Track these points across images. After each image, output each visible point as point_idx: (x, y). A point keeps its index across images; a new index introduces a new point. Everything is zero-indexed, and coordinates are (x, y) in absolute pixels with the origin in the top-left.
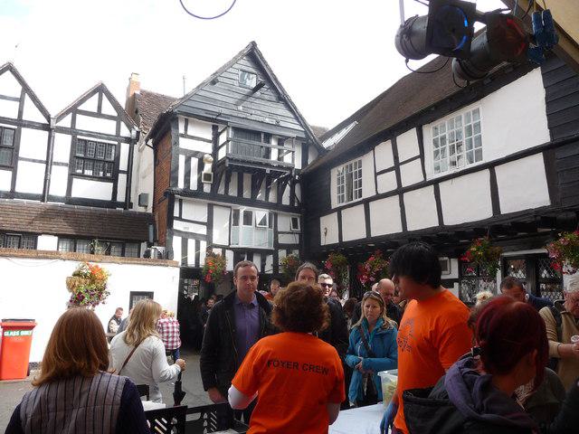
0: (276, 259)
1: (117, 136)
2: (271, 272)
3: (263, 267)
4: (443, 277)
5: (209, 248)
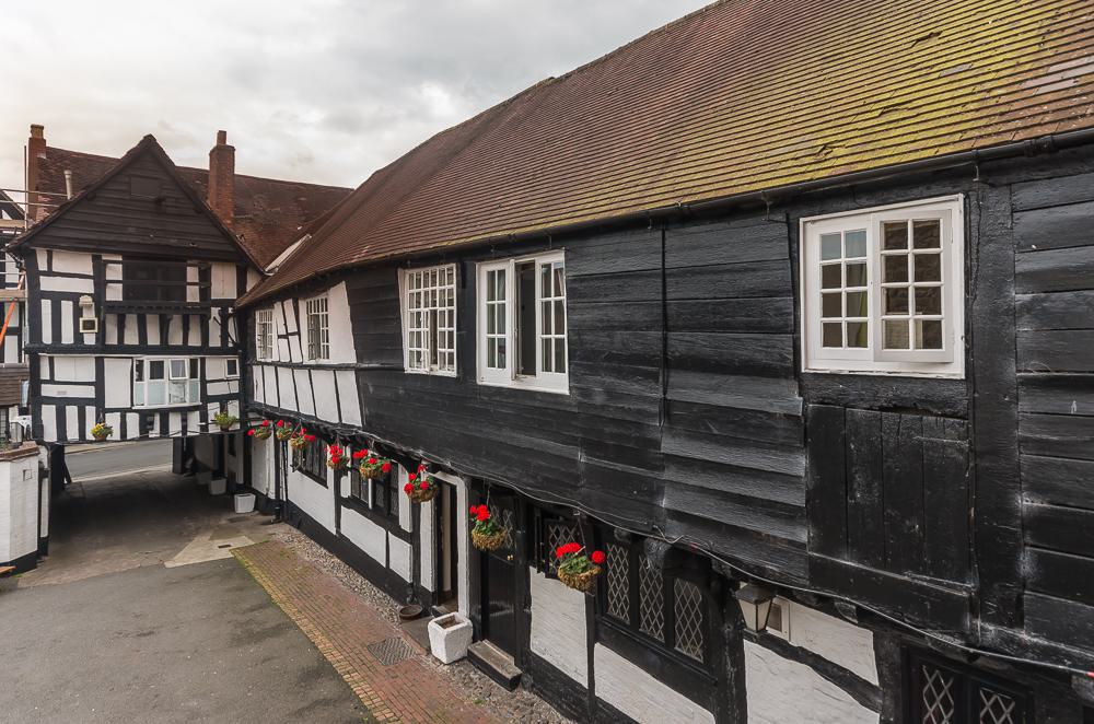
0: (204, 417)
3: (185, 429)
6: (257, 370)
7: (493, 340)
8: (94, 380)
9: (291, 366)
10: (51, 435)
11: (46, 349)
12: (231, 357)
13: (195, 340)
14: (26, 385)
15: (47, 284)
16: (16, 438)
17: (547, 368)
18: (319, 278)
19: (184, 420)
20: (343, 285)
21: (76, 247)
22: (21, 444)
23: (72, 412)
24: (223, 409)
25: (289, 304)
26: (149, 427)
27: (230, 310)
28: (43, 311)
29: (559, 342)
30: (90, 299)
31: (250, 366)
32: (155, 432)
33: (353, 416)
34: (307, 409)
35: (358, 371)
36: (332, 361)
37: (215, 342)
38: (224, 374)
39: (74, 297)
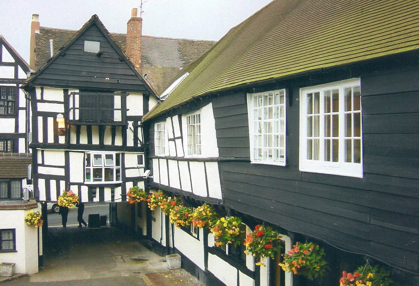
0: (124, 190)
1: (16, 80)
2: (120, 200)
3: (113, 197)
4: (165, 246)
5: (68, 188)
6: (155, 162)
7: (329, 141)
8: (64, 165)
9: (178, 159)
10: (43, 197)
11: (40, 145)
12: (140, 153)
13: (119, 142)
14: (30, 167)
15: (41, 107)
16: (26, 198)
17: (348, 160)
18: (195, 101)
19: (113, 192)
20: (210, 105)
21: (55, 85)
22: (29, 201)
23: (53, 183)
24: (135, 184)
25: (175, 118)
26: (93, 195)
27: (139, 123)
28: (39, 124)
29: (357, 142)
30: (62, 116)
31: (151, 159)
32: (97, 199)
33: (216, 193)
34: (186, 188)
35: (221, 162)
36: (204, 156)
37: (130, 143)
38: (135, 163)
39: (54, 115)
